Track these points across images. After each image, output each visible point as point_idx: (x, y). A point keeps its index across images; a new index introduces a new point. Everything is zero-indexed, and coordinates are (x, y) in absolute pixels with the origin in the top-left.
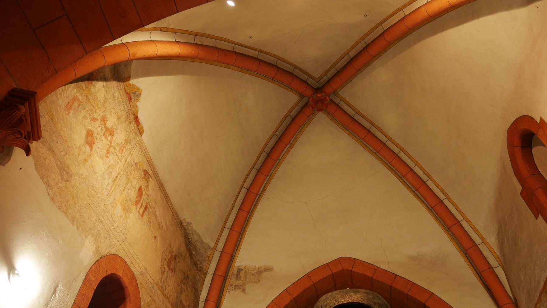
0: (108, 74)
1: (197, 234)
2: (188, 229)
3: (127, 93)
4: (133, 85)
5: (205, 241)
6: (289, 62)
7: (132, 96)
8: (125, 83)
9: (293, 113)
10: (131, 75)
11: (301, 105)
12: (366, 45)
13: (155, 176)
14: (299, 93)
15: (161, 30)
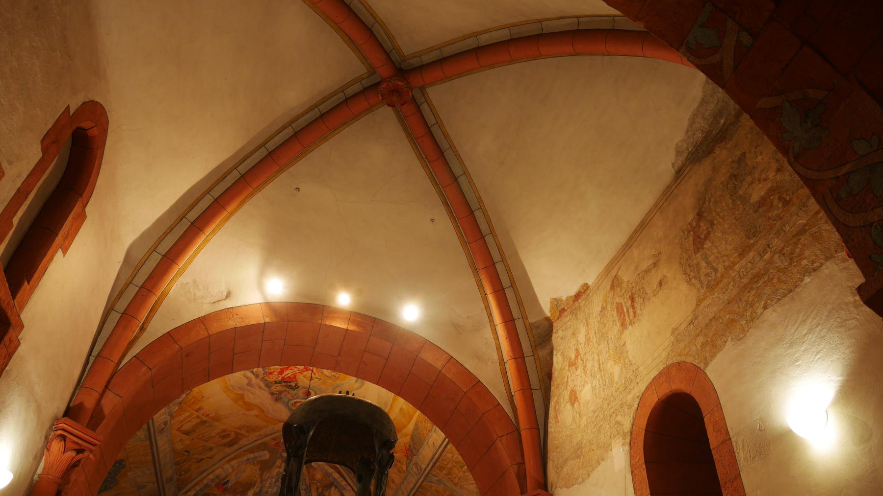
0: (548, 349)
1: (692, 122)
2: (688, 149)
3: (560, 315)
4: (551, 311)
5: (700, 95)
6: (413, 149)
7: (560, 308)
8: (553, 321)
9: (350, 91)
10: (543, 317)
11: (366, 83)
12: (576, 28)
13: (620, 259)
14: (423, 95)
15: (491, 315)
